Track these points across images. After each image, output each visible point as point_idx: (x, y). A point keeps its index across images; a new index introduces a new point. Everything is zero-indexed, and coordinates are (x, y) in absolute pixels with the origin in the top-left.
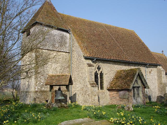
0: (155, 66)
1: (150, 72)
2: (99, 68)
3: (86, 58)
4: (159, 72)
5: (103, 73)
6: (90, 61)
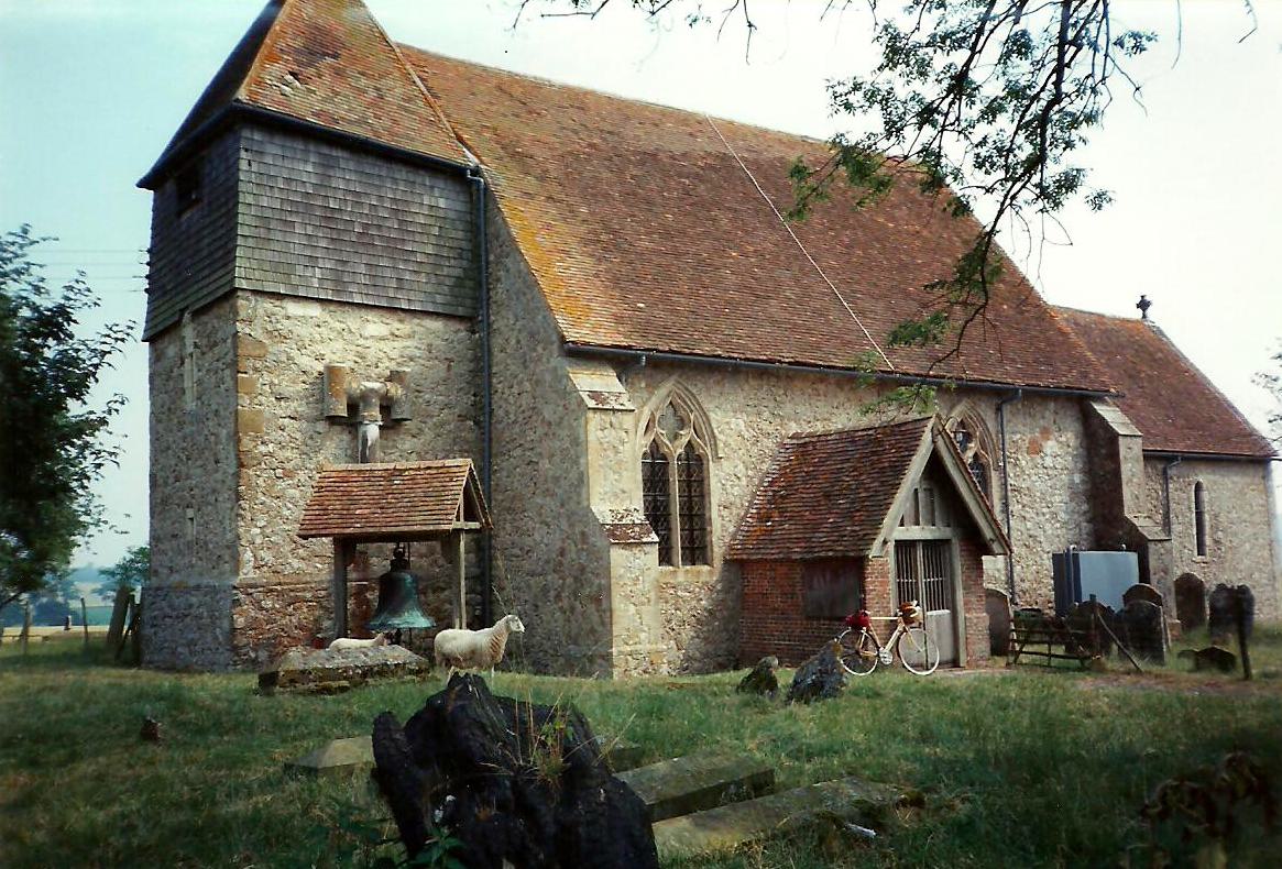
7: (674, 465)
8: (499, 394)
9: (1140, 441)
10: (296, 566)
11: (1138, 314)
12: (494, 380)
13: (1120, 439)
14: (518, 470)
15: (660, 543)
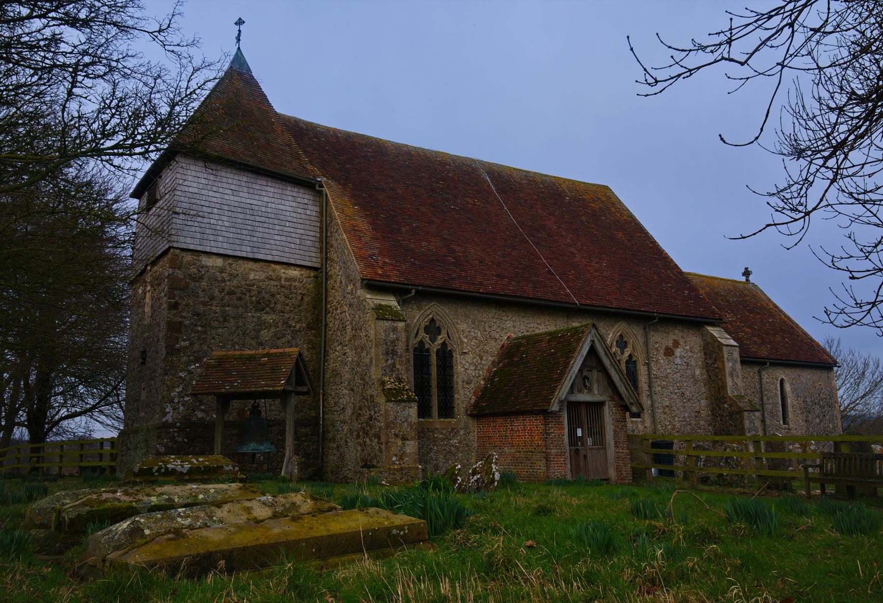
0: (696, 323)
1: (669, 352)
2: (433, 329)
3: (373, 286)
4: (712, 351)
5: (450, 351)
6: (392, 298)
7: (434, 359)
8: (330, 314)
9: (737, 349)
10: (199, 416)
11: (743, 279)
12: (329, 306)
13: (724, 347)
14: (339, 358)
15: (418, 402)
